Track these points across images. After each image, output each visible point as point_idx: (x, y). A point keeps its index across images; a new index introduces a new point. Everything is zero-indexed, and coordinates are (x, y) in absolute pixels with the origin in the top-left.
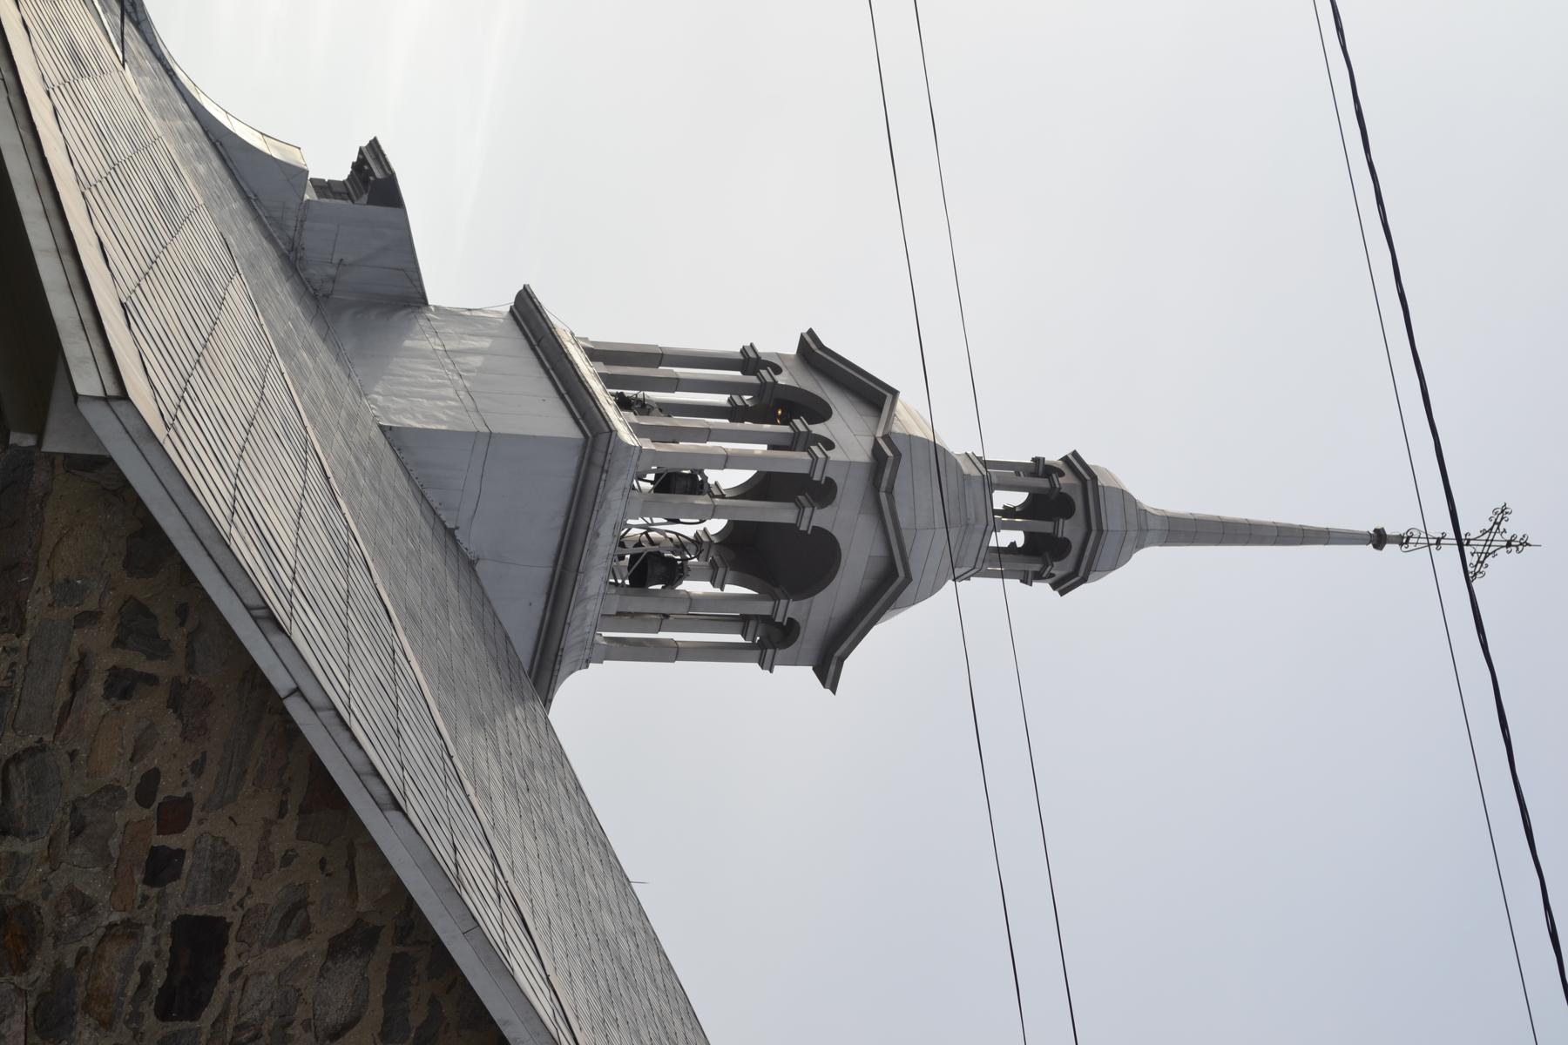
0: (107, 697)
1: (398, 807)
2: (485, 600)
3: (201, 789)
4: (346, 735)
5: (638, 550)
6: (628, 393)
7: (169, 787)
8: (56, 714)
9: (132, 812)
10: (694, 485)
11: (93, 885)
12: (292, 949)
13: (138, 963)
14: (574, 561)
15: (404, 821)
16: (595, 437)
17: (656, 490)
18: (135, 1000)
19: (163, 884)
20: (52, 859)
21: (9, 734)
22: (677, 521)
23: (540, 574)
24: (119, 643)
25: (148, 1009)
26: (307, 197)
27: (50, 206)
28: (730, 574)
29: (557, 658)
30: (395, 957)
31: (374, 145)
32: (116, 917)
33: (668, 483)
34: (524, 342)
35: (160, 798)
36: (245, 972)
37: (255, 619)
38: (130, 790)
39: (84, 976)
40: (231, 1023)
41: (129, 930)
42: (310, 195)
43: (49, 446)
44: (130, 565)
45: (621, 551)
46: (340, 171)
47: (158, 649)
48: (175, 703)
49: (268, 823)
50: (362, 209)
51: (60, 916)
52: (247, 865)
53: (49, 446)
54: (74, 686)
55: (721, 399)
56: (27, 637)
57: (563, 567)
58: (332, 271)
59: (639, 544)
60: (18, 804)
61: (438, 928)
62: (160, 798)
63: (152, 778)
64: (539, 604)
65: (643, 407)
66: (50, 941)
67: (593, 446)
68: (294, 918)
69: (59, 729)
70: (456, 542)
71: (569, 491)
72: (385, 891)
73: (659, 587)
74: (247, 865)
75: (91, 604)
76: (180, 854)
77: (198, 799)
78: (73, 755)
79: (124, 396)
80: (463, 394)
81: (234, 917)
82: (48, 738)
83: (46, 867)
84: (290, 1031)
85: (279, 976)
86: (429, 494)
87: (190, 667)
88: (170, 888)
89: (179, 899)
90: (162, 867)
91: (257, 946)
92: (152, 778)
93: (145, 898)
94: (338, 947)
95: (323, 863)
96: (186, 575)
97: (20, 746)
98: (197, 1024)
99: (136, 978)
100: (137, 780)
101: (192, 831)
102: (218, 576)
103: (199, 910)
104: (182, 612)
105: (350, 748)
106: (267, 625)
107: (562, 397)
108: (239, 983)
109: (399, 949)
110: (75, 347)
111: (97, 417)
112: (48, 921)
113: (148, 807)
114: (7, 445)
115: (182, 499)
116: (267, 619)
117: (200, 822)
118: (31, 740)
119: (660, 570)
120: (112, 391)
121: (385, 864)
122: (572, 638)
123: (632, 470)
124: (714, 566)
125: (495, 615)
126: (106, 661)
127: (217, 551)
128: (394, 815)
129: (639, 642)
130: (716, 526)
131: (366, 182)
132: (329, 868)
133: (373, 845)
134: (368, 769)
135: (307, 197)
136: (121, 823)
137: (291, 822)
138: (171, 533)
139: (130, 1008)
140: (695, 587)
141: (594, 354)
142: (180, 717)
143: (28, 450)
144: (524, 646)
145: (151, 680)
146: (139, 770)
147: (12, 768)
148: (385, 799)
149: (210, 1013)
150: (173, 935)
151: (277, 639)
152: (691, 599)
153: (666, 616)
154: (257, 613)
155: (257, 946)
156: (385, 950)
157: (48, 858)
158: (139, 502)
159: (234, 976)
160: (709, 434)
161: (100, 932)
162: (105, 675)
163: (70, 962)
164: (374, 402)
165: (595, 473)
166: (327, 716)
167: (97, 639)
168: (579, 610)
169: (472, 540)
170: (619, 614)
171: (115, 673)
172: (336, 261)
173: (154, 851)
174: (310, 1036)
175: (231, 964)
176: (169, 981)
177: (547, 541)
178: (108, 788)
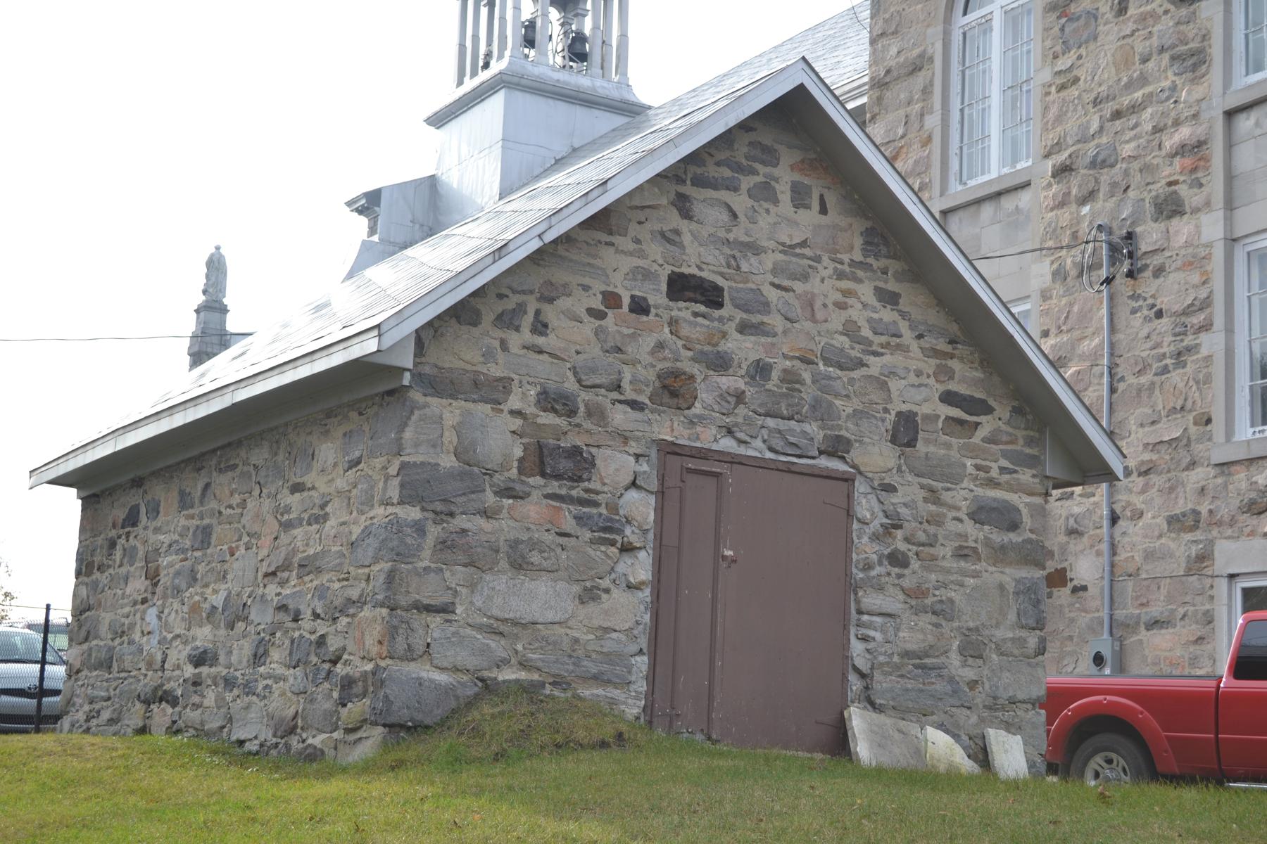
0: (547, 335)
1: (606, 182)
2: (593, 142)
3: (598, 286)
4: (565, 210)
5: (567, 58)
6: (481, 63)
7: (597, 303)
8: (556, 361)
9: (609, 322)
10: (531, 26)
11: (648, 342)
12: (687, 238)
13: (692, 318)
14: (573, 93)
15: (613, 180)
16: (504, 82)
17: (533, 47)
18: (712, 320)
19: (649, 306)
20: (634, 362)
21: (566, 385)
22: (551, 36)
23: (580, 113)
24: (517, 329)
25: (717, 313)
26: (377, 240)
27: (291, 366)
28: (581, 6)
29: (626, 102)
30: (693, 184)
31: (349, 204)
32: (667, 330)
33: (530, 42)
34: (453, 121)
35: (602, 308)
36: (698, 263)
37: (500, 258)
38: (598, 323)
39: (698, 347)
40: (726, 270)
41: (673, 323)
42: (375, 238)
43: (410, 366)
44: (475, 324)
45: (567, 67)
46: (363, 222)
47: (521, 309)
48: (551, 300)
49: (617, 251)
50: (383, 210)
51: (665, 359)
52: (641, 263)
53: (410, 366)
54: (541, 352)
55: (484, 11)
56: (513, 376)
57: (576, 99)
58: (417, 226)
59: (564, 57)
60: (604, 380)
61: (673, 161)
62: (602, 308)
63: (591, 312)
64: (596, 112)
65: (489, 55)
66: (678, 363)
67: (509, 83)
68: (670, 238)
69: (563, 360)
70: (563, 158)
71: (534, 96)
72: (656, 190)
73: (587, 46)
74: (641, 263)
75: (497, 344)
76: (633, 297)
77: (603, 288)
78: (578, 353)
79: (378, 326)
80: (482, 155)
81: (668, 269)
82: (568, 365)
83: (639, 366)
84: (731, 240)
85: (701, 245)
86: (536, 173)
87: (531, 292)
88: (651, 302)
89: (657, 296)
90: (640, 307)
91: (684, 257)
92: (591, 312)
93: (657, 315)
94: (686, 215)
95: (640, 223)
96: (475, 294)
97: (573, 379)
98: (726, 288)
99: (700, 320)
100: (592, 320)
101: (620, 291)
102: (476, 277)
103: (664, 287)
104: (501, 296)
105: (572, 208)
106: (504, 251)
107: (483, 100)
108: (704, 266)
109: (688, 182)
110: (357, 351)
111: (389, 341)
112: (668, 365)
113: (606, 314)
114: (410, 387)
115: (434, 296)
116: (501, 251)
117: (616, 287)
118: (570, 374)
119: (578, 47)
120: (375, 333)
121: (639, 189)
122: (615, 94)
123: (522, 61)
124: (577, 15)
125: (601, 137)
126: (527, 336)
127: (462, 278)
128: (610, 184)
129: (618, 57)
130: (554, 14)
131: (368, 208)
132: (643, 219)
133: (630, 195)
134: (584, 199)
135: (377, 240)
136: (616, 328)
137: (617, 239)
138: (453, 302)
139: (716, 323)
140: (588, 26)
141: (460, 82)
142: (558, 297)
143: (413, 376)
144: (619, 120)
145: (538, 313)
146: (586, 318)
147: (584, 383)
148: (600, 190)
149: (720, 281)
150: (677, 301)
151: (511, 246)
152: (595, 27)
153: (604, 42)
154: (497, 258)
155: (684, 257)
156: (688, 189)
157: (634, 365)
158: (439, 317)
159: (700, 269)
160: (503, 19)
161: (674, 338)
162: (535, 336)
163: (690, 354)
164: (486, 203)
165: (523, 82)
166: (554, 220)
167: (515, 340)
168: (600, 90)
169: (561, 149)
170: (602, 68)
171: (534, 331)
172: (411, 224)
173: (631, 310)
174: (735, 229)
175: (694, 271)
176: (701, 303)
177: (562, 107)
178: (596, 334)
